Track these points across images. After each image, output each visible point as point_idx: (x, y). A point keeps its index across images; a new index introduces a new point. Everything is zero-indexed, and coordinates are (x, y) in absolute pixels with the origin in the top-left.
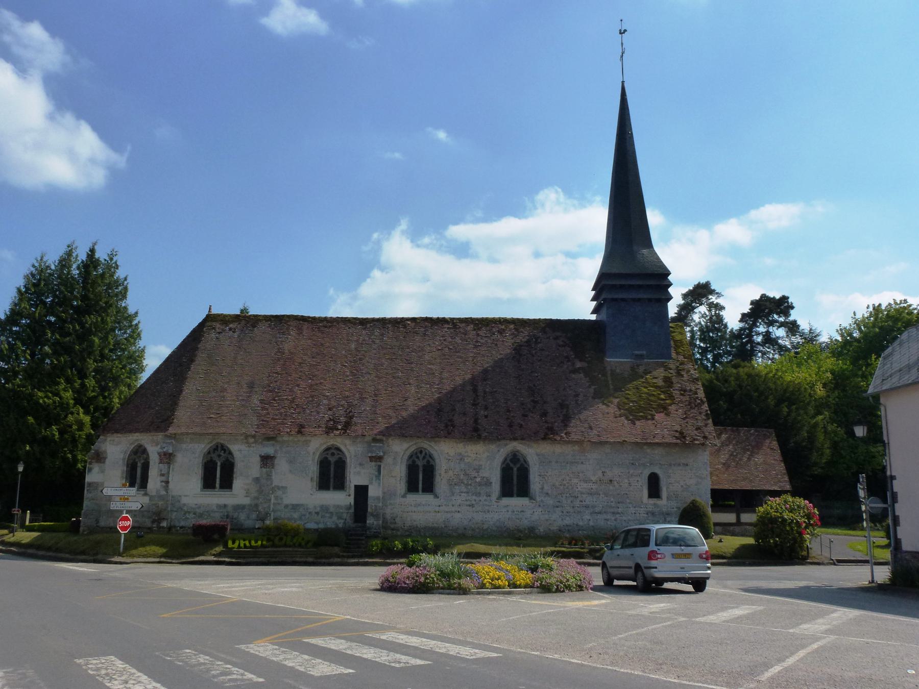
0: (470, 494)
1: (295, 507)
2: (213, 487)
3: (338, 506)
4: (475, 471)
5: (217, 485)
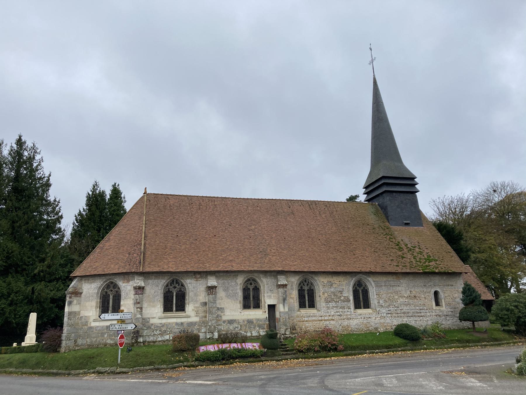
0: (339, 308)
1: (231, 322)
2: (305, 307)
3: (258, 320)
4: (340, 293)
5: (174, 309)
